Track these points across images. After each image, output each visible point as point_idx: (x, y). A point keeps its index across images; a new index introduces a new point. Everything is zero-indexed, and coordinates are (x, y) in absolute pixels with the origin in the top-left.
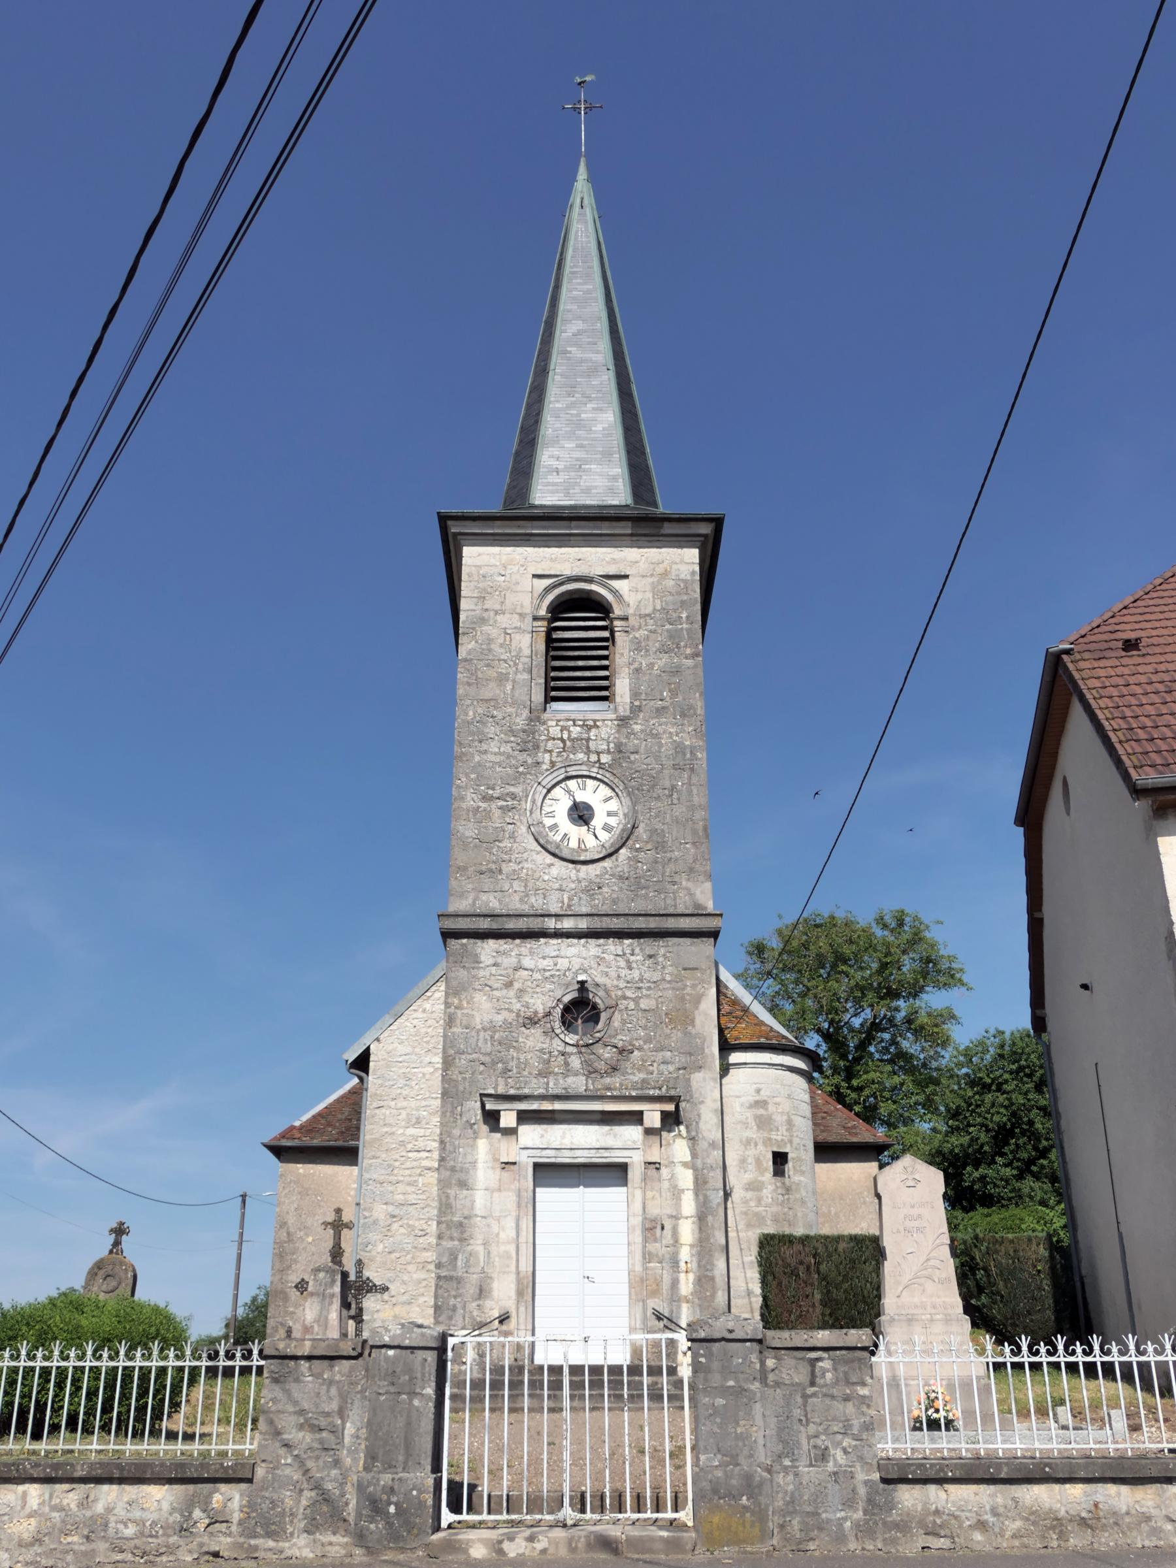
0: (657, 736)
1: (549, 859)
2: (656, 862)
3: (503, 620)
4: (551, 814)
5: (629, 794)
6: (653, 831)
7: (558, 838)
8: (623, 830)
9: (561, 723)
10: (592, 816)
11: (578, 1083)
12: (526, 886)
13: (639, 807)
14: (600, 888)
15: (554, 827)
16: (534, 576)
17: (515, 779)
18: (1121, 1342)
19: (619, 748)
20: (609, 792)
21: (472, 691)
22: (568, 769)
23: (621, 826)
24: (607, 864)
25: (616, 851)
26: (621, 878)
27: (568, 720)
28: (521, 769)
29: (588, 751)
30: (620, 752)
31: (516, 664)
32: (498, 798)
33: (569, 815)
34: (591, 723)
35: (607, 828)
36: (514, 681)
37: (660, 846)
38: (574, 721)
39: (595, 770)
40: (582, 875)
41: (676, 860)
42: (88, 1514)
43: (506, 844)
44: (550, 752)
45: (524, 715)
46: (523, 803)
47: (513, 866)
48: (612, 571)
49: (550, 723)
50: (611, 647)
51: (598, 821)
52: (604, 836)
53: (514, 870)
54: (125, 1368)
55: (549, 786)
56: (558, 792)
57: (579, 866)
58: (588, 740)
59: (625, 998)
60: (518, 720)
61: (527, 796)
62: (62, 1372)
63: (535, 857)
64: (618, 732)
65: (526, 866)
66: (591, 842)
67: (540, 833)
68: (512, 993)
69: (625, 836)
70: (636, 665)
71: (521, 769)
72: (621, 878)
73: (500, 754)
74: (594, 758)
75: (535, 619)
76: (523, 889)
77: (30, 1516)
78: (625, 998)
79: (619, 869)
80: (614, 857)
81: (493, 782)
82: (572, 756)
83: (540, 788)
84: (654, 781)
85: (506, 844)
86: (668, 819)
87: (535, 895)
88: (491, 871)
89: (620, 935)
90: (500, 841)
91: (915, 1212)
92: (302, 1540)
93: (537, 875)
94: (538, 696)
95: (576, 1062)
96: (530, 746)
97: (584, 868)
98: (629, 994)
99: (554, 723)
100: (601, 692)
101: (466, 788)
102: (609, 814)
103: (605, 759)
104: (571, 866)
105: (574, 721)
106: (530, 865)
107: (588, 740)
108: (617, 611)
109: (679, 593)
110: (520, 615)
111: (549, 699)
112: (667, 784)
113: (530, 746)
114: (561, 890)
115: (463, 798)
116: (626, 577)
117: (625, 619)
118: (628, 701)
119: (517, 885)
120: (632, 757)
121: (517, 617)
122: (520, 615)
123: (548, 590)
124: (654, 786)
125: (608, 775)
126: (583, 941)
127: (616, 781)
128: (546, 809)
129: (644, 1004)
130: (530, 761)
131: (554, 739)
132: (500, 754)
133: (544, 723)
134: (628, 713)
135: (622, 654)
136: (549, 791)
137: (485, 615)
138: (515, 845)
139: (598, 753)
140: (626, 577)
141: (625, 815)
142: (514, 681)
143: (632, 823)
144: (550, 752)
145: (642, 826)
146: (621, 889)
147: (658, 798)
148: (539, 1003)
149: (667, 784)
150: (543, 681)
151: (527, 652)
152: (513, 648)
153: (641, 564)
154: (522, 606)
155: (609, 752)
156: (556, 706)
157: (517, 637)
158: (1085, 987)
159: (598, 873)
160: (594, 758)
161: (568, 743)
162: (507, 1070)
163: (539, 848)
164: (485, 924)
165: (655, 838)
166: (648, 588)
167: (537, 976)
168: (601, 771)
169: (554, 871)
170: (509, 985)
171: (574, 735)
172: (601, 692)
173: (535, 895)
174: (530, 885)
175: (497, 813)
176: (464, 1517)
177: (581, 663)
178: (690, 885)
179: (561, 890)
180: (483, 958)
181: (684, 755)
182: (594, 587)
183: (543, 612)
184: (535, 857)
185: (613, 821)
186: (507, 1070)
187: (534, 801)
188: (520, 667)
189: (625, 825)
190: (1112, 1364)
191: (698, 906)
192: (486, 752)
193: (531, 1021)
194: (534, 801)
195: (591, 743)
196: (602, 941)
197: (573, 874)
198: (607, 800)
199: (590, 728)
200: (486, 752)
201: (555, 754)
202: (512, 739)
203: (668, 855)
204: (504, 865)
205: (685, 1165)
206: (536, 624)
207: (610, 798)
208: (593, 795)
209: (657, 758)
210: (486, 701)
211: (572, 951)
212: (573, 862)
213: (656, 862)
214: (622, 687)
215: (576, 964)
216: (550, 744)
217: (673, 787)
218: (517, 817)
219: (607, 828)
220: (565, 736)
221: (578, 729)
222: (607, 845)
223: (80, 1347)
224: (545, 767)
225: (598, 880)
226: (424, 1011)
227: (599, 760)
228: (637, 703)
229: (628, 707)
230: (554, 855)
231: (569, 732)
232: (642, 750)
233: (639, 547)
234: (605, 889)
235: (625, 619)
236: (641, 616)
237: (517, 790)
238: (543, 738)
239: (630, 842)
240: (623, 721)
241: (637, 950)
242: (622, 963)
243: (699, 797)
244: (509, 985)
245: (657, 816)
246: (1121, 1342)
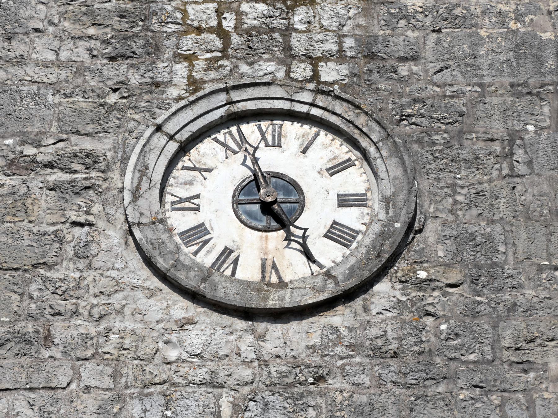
1: (182, 308)
2: (475, 315)
4: (190, 204)
5: (396, 151)
6: (465, 240)
7: (207, 259)
8: (382, 236)
10: (300, 205)
12: (115, 376)
13: (424, 184)
14: (319, 379)
15: (198, 234)
17: (97, 120)
19: (369, 52)
20: (341, 150)
22: (236, 96)
23: (376, 227)
24: (340, 317)
25: (365, 287)
26: (378, 353)
28: (112, 99)
29: (288, 55)
30: (371, 56)
32: (50, 165)
33: (237, 203)
35: (337, 233)
37: (485, 275)
39: (307, 97)
40: (270, 346)
41: (530, 309)
43: (67, 271)
44: (190, 58)
46: (115, 175)
47: (83, 326)
51: (314, 219)
52: (329, 253)
53: (86, 337)
55: (185, 135)
56: (206, 151)
57: (261, 326)
58: (288, 30)
61: (125, 159)
63: (143, 302)
65: (118, 325)
66: (294, 267)
67: (159, 244)
69: (388, 249)
71: (112, 99)
72: (378, 353)
73: (58, 64)
74: (302, 71)
76: (107, 382)
79: (374, 331)
80: (358, 303)
81: (38, 126)
82: (244, 68)
83: (160, 140)
84: (460, 123)
85: (67, 271)
86: (503, 210)
87: (142, 397)
88: (25, 339)
90: (50, 266)
93: (146, 349)
96: (137, 46)
97: (275, 330)
102: (344, 201)
103: (330, 73)
104: (240, 324)
106: (129, 325)
107: (288, 30)
112: (497, 128)
113: (137, 46)
114: (212, 383)
119: (90, 373)
120: (403, 70)
124: (462, 133)
125: (339, 107)
127: (361, 120)
128: (176, 190)
130: (135, 79)
131: (199, 30)
132: (58, 64)
136: (184, 148)
138: (90, 275)
139: (314, 61)
141: (387, 201)
143: (405, 217)
144: (190, 58)
145: (431, 232)
146: (379, 382)
147: (474, 162)
149: (497, 128)
155: (340, 56)
159: (315, 340)
160: (302, 71)
161: (236, 40)
163: (155, 282)
165: (468, 254)
168: (321, 101)
169: (195, 338)
171: (249, 22)
173: (142, 397)
174: (129, 371)
175: (45, 200)
179: (212, 383)
181: (540, 61)
184: (143, 302)
185: (352, 217)
187: (143, 171)
189: (388, 224)
192: (21, 61)
194: (143, 171)
195: (294, 39)
197: (247, 345)
200: (21, 61)
201: (200, 64)
202: (92, 31)
203: (507, 297)
204: (58, 324)
207: (346, 165)
208: (301, 156)
209: (470, 65)
212: (247, 314)
213: (475, 315)
216: (188, 42)
217: (513, 137)
218: (96, 208)
219: (337, 233)
220: (229, 23)
222: (339, 273)
224: (174, 92)
225: (315, 360)
227: (316, 77)
230: (195, 297)
231: (239, 14)
232: (428, 53)
233: (163, 283)
234: (335, 383)
237: (102, 146)
239: (402, 266)
245: (472, 204)
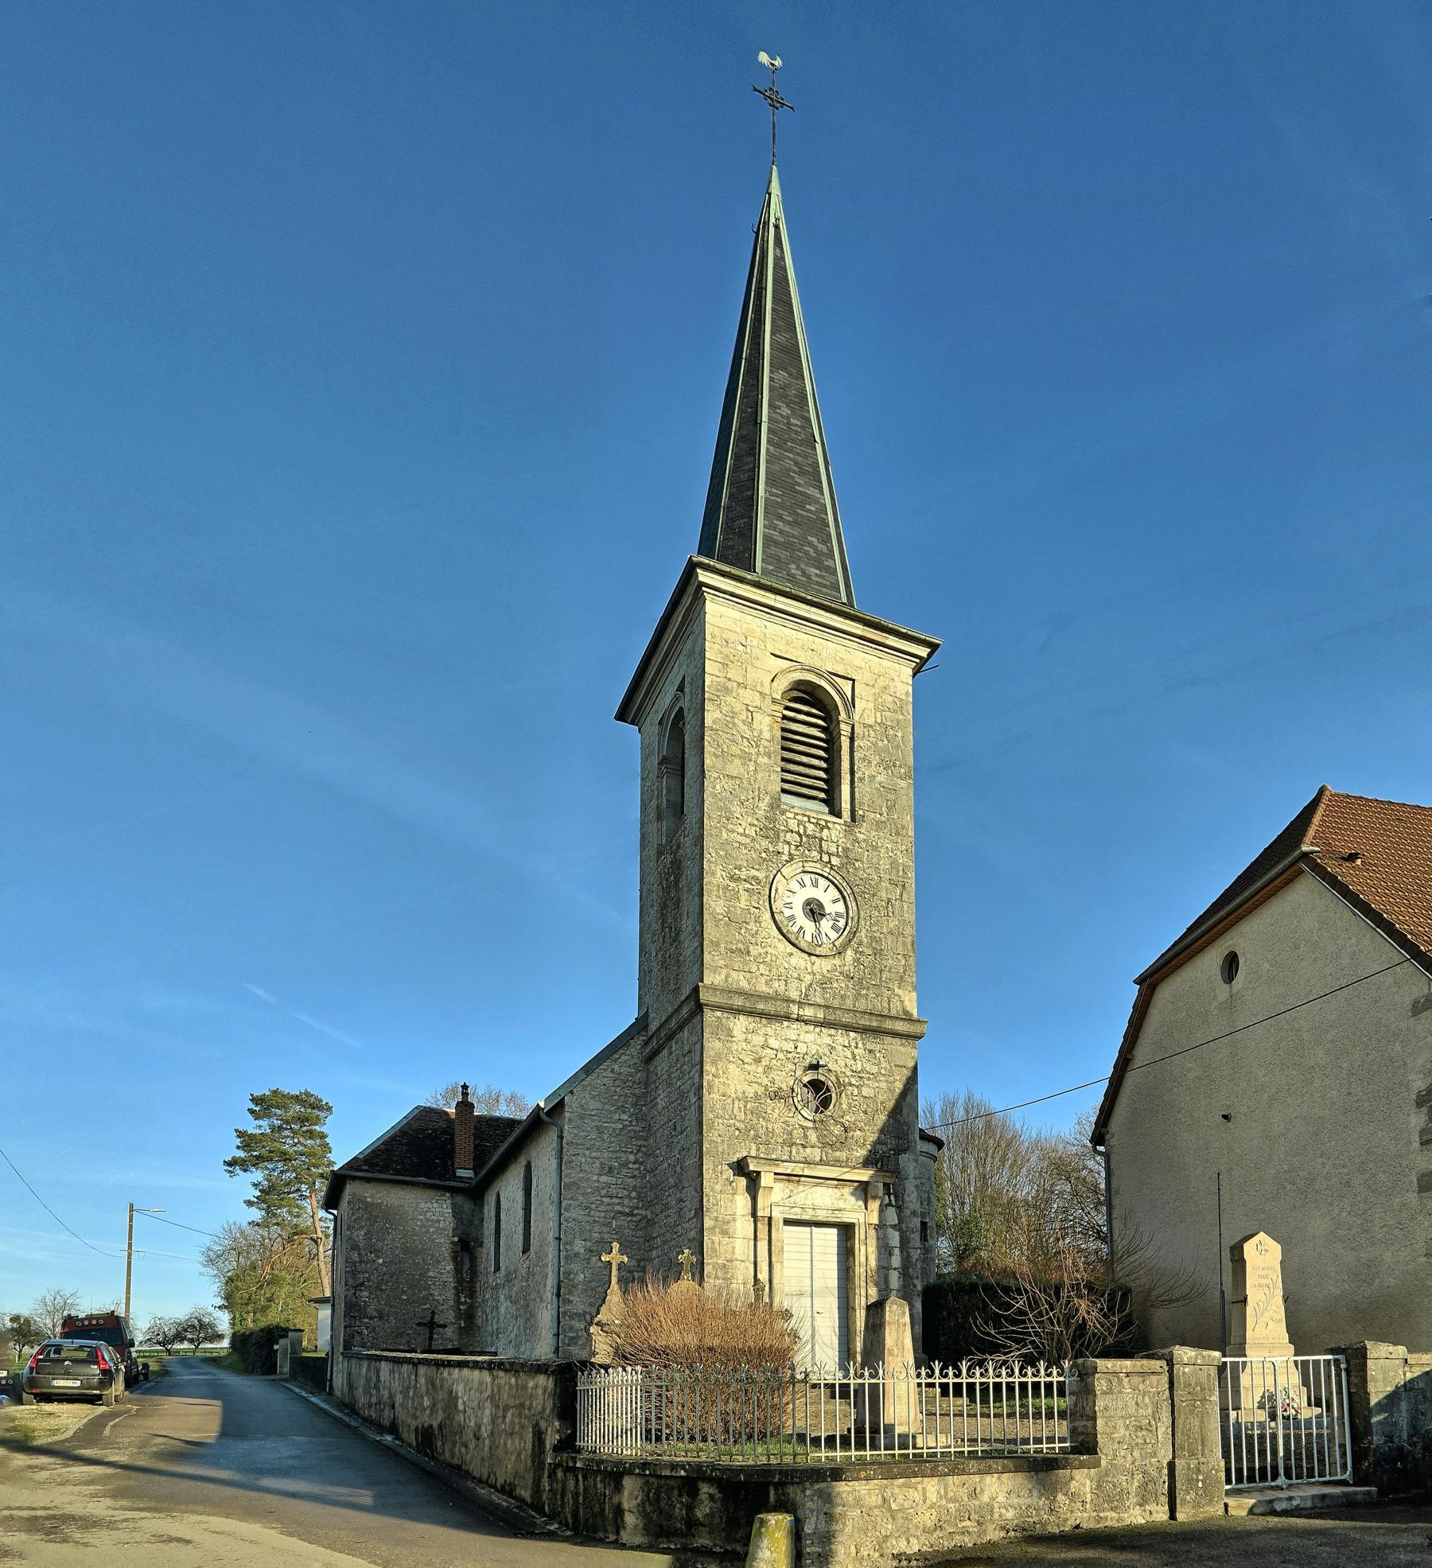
0: (875, 848)
3: (748, 696)
7: (795, 929)
11: (815, 1154)
15: (792, 918)
18: (956, 1367)
21: (719, 763)
42: (977, 1503)
54: (981, 1384)
59: (851, 1085)
62: (998, 1386)
68: (760, 1069)
77: (931, 1507)
78: (851, 1085)
89: (847, 1028)
91: (1265, 1273)
92: (1137, 1510)
95: (813, 1137)
98: (853, 1081)
101: (716, 864)
103: (835, 861)
109: (895, 712)
115: (714, 874)
126: (818, 1029)
129: (866, 1092)
137: (729, 684)
139: (829, 854)
148: (783, 1080)
155: (838, 856)
158: (1225, 1117)
160: (825, 858)
162: (757, 1136)
164: (738, 1002)
166: (871, 698)
167: (781, 1056)
169: (794, 961)
170: (758, 1061)
176: (1294, 1481)
177: (805, 759)
178: (900, 992)
180: (735, 1033)
186: (757, 1136)
190: (974, 1384)
191: (906, 1012)
193: (776, 1095)
196: (833, 1031)
198: (835, 901)
200: (733, 831)
205: (894, 1227)
210: (732, 777)
211: (809, 1038)
215: (813, 1049)
223: (1033, 1365)
226: (612, 1071)
241: (860, 1045)
242: (849, 1055)
243: (910, 915)
244: (758, 1061)
246: (956, 1367)
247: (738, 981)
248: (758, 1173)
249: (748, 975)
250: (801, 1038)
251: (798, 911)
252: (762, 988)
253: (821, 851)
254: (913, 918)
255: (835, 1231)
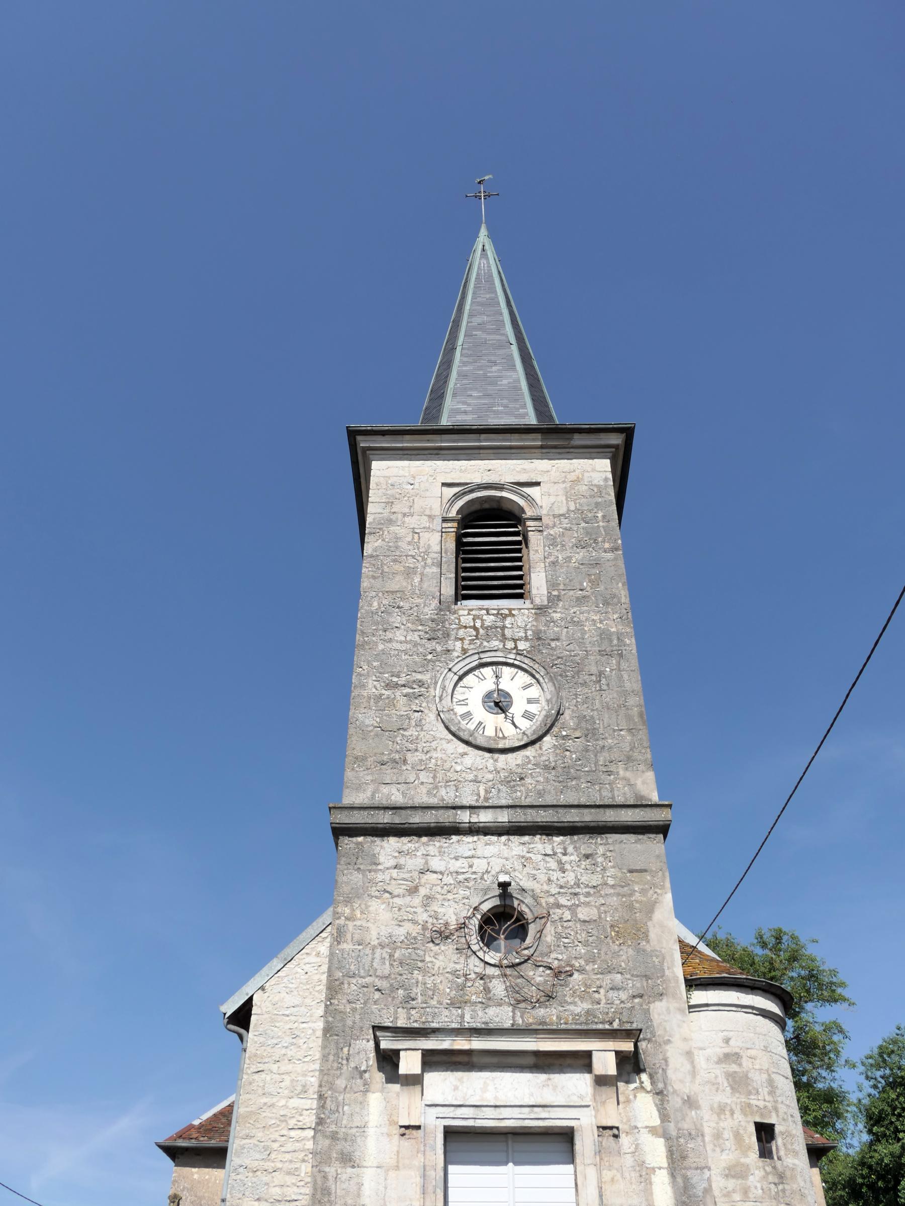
0: (578, 623)
9: (473, 612)
11: (503, 1016)
15: (468, 715)
16: (444, 484)
27: (481, 609)
31: (424, 559)
34: (507, 612)
36: (422, 574)
38: (487, 610)
45: (433, 607)
48: (523, 479)
49: (461, 612)
50: (524, 550)
59: (558, 906)
60: (426, 610)
64: (536, 620)
68: (417, 901)
70: (552, 559)
75: (445, 520)
94: (449, 589)
95: (498, 988)
98: (563, 901)
99: (466, 612)
100: (516, 590)
103: (522, 645)
105: (487, 610)
108: (529, 513)
110: (430, 516)
111: (459, 597)
115: (363, 686)
116: (538, 484)
117: (539, 519)
118: (546, 592)
121: (426, 518)
122: (430, 516)
123: (457, 496)
131: (466, 627)
133: (455, 613)
134: (546, 603)
135: (537, 551)
139: (515, 641)
140: (538, 484)
142: (422, 574)
150: (453, 575)
151: (438, 548)
152: (422, 544)
153: (552, 472)
154: (431, 509)
155: (526, 639)
156: (465, 602)
157: (425, 536)
164: (386, 818)
167: (448, 880)
169: (468, 761)
171: (487, 624)
172: (516, 590)
180: (382, 859)
182: (504, 494)
183: (453, 513)
188: (429, 561)
193: (442, 935)
199: (505, 617)
200: (390, 640)
205: (653, 1130)
206: (445, 525)
210: (392, 592)
214: (538, 582)
220: (478, 624)
221: (492, 617)
228: (555, 593)
229: (545, 599)
231: (482, 620)
235: (539, 519)
236: (554, 516)
238: (454, 626)
240: (541, 610)
241: (570, 849)
242: (553, 864)
247: (389, 796)
248: (396, 1053)
249: (402, 787)
250: (479, 853)
251: (480, 714)
252: (422, 798)
253: (504, 638)
254: (637, 686)
255: (451, 1168)
